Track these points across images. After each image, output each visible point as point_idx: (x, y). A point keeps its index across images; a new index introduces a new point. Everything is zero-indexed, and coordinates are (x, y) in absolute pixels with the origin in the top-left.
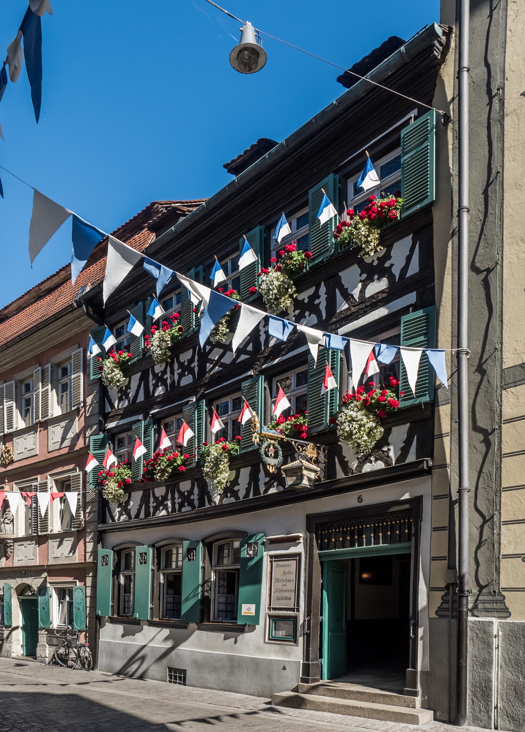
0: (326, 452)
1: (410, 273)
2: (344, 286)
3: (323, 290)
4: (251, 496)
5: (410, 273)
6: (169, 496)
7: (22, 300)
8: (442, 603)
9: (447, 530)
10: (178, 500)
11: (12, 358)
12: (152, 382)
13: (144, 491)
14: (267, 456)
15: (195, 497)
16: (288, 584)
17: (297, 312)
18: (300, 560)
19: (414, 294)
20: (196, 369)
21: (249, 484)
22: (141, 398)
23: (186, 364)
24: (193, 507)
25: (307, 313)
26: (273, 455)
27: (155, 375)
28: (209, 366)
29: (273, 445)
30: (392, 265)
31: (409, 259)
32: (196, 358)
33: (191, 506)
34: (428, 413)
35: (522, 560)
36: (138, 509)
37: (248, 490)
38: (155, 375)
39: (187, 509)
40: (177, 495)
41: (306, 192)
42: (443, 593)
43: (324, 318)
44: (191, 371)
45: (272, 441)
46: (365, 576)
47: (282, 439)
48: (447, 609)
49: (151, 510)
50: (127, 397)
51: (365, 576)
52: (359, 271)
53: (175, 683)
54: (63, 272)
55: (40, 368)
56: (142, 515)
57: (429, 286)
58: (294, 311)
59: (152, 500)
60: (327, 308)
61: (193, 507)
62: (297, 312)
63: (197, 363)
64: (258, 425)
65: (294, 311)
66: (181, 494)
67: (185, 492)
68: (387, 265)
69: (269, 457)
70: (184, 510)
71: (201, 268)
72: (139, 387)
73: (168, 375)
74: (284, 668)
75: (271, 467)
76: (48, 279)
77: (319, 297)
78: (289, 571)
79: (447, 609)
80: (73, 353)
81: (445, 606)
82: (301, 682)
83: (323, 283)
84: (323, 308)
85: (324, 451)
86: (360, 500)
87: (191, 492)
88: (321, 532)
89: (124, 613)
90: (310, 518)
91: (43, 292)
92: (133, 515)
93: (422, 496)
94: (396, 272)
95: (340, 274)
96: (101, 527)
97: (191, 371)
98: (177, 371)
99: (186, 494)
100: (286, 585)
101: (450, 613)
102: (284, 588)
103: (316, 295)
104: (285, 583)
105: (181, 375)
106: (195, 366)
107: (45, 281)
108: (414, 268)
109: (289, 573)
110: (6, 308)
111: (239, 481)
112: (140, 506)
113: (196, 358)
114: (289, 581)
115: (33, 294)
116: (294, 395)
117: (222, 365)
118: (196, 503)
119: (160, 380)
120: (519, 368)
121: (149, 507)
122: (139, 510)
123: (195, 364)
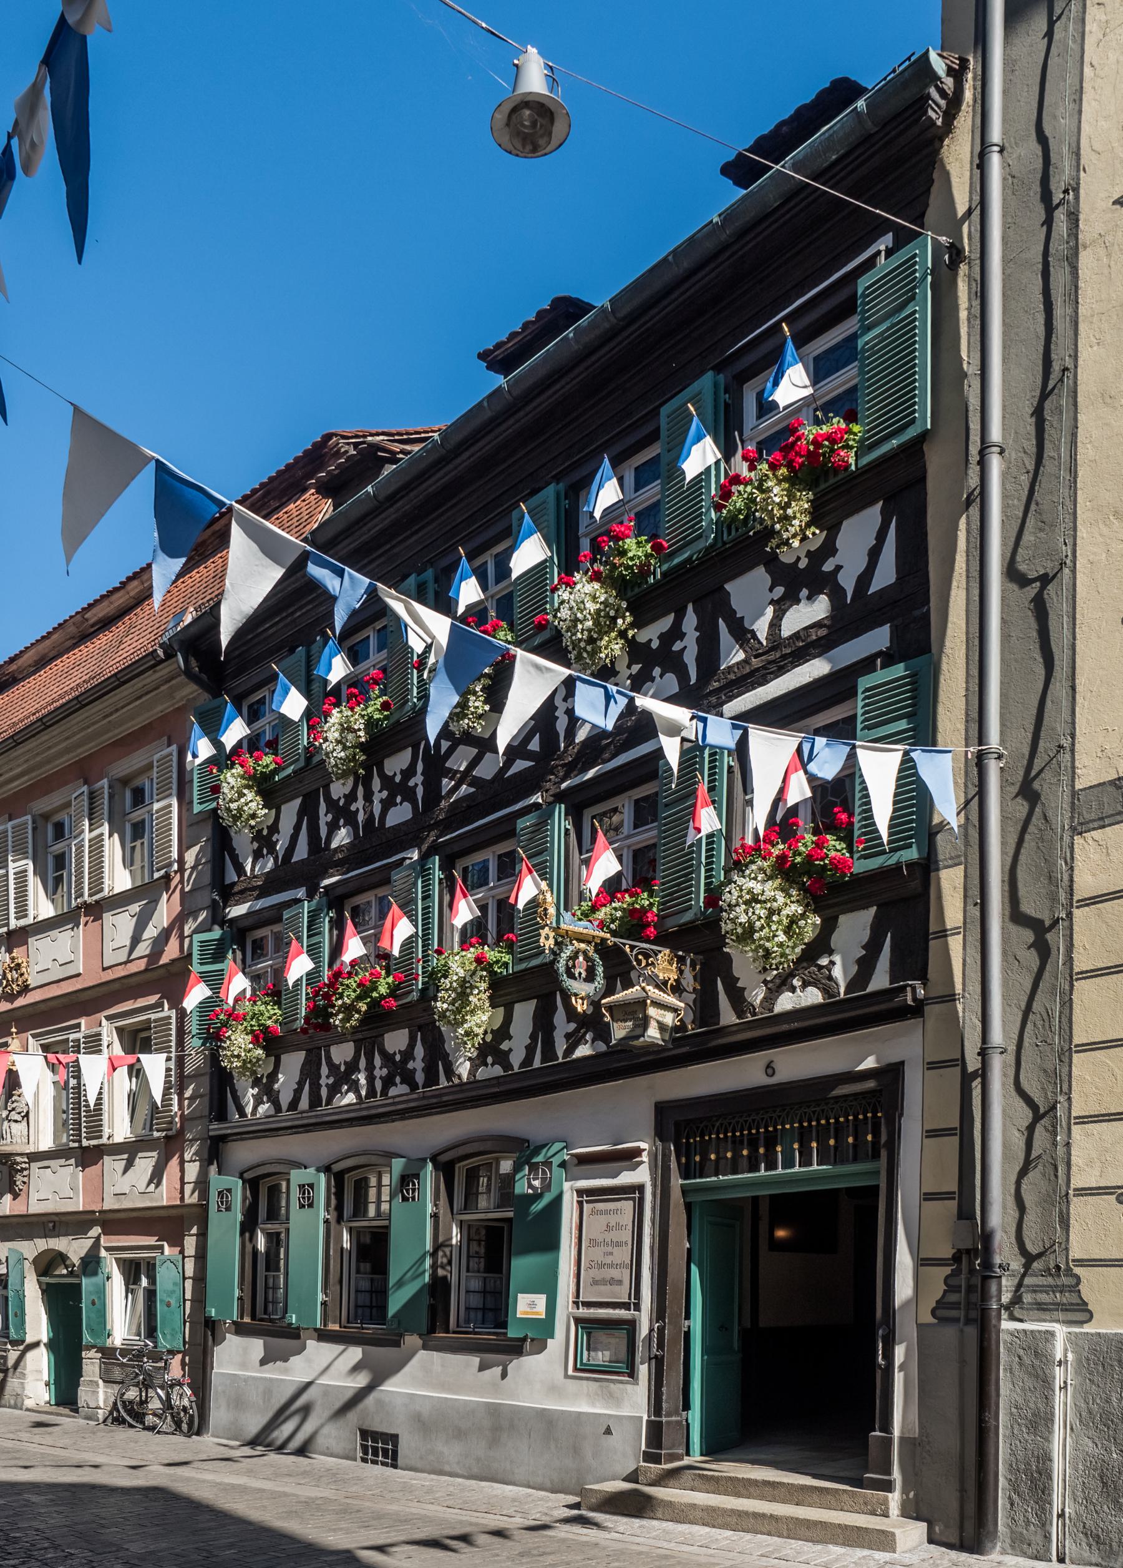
0: (698, 967)
1: (877, 584)
2: (735, 612)
3: (690, 620)
4: (537, 1063)
5: (877, 584)
6: (363, 1063)
7: (48, 642)
8: (945, 1292)
9: (955, 1134)
10: (380, 1072)
11: (25, 766)
12: (324, 818)
13: (309, 1051)
14: (571, 976)
15: (417, 1064)
16: (616, 1250)
17: (636, 668)
18: (641, 1200)
19: (886, 629)
20: (420, 791)
21: (533, 1037)
22: (302, 852)
23: (398, 779)
24: (414, 1086)
25: (657, 671)
26: (584, 975)
27: (332, 804)
28: (447, 784)
29: (585, 953)
30: (839, 568)
31: (874, 554)
32: (420, 767)
33: (409, 1085)
34: (915, 885)
35: (1117, 1199)
36: (296, 1091)
37: (530, 1050)
38: (332, 804)
39: (399, 1089)
40: (378, 1061)
41: (655, 412)
42: (947, 1270)
43: (693, 681)
44: (409, 795)
45: (583, 946)
46: (781, 1233)
47: (603, 940)
48: (955, 1306)
49: (324, 1092)
50: (272, 850)
51: (781, 1233)
52: (768, 580)
53: (374, 1462)
54: (135, 583)
55: (85, 788)
56: (304, 1104)
57: (917, 613)
58: (629, 667)
59: (324, 1070)
60: (699, 660)
61: (414, 1086)
62: (636, 668)
63: (422, 778)
64: (552, 911)
65: (629, 667)
66: (387, 1058)
67: (395, 1053)
68: (828, 567)
69: (575, 979)
70: (393, 1092)
71: (429, 574)
72: (297, 828)
73: (359, 804)
74: (608, 1431)
75: (580, 1001)
76: (103, 597)
77: (682, 636)
78: (618, 1224)
79: (955, 1306)
80: (156, 757)
81: (953, 1298)
82: (644, 1461)
83: (690, 607)
84: (690, 659)
85: (693, 965)
86: (770, 1071)
87: (408, 1055)
88: (688, 1139)
89: (265, 1313)
90: (662, 1110)
91: (92, 626)
92: (284, 1104)
93: (902, 1063)
94: (848, 582)
95: (728, 587)
96: (217, 1129)
97: (409, 795)
98: (379, 796)
99: (398, 1058)
100: (611, 1253)
101: (963, 1313)
102: (608, 1260)
103: (676, 633)
104: (610, 1249)
105: (387, 804)
106: (416, 785)
107: (96, 601)
108: (886, 575)
109: (619, 1227)
110: (12, 660)
111: (512, 1031)
112: (300, 1085)
113: (420, 767)
114: (619, 1244)
115: (71, 629)
116: (629, 847)
117: (476, 782)
118: (420, 1077)
119: (342, 813)
120: (1111, 789)
121: (320, 1086)
122: (298, 1093)
123: (418, 779)
